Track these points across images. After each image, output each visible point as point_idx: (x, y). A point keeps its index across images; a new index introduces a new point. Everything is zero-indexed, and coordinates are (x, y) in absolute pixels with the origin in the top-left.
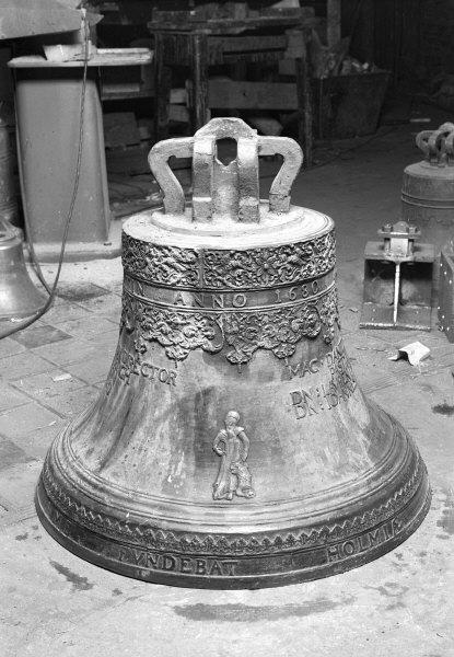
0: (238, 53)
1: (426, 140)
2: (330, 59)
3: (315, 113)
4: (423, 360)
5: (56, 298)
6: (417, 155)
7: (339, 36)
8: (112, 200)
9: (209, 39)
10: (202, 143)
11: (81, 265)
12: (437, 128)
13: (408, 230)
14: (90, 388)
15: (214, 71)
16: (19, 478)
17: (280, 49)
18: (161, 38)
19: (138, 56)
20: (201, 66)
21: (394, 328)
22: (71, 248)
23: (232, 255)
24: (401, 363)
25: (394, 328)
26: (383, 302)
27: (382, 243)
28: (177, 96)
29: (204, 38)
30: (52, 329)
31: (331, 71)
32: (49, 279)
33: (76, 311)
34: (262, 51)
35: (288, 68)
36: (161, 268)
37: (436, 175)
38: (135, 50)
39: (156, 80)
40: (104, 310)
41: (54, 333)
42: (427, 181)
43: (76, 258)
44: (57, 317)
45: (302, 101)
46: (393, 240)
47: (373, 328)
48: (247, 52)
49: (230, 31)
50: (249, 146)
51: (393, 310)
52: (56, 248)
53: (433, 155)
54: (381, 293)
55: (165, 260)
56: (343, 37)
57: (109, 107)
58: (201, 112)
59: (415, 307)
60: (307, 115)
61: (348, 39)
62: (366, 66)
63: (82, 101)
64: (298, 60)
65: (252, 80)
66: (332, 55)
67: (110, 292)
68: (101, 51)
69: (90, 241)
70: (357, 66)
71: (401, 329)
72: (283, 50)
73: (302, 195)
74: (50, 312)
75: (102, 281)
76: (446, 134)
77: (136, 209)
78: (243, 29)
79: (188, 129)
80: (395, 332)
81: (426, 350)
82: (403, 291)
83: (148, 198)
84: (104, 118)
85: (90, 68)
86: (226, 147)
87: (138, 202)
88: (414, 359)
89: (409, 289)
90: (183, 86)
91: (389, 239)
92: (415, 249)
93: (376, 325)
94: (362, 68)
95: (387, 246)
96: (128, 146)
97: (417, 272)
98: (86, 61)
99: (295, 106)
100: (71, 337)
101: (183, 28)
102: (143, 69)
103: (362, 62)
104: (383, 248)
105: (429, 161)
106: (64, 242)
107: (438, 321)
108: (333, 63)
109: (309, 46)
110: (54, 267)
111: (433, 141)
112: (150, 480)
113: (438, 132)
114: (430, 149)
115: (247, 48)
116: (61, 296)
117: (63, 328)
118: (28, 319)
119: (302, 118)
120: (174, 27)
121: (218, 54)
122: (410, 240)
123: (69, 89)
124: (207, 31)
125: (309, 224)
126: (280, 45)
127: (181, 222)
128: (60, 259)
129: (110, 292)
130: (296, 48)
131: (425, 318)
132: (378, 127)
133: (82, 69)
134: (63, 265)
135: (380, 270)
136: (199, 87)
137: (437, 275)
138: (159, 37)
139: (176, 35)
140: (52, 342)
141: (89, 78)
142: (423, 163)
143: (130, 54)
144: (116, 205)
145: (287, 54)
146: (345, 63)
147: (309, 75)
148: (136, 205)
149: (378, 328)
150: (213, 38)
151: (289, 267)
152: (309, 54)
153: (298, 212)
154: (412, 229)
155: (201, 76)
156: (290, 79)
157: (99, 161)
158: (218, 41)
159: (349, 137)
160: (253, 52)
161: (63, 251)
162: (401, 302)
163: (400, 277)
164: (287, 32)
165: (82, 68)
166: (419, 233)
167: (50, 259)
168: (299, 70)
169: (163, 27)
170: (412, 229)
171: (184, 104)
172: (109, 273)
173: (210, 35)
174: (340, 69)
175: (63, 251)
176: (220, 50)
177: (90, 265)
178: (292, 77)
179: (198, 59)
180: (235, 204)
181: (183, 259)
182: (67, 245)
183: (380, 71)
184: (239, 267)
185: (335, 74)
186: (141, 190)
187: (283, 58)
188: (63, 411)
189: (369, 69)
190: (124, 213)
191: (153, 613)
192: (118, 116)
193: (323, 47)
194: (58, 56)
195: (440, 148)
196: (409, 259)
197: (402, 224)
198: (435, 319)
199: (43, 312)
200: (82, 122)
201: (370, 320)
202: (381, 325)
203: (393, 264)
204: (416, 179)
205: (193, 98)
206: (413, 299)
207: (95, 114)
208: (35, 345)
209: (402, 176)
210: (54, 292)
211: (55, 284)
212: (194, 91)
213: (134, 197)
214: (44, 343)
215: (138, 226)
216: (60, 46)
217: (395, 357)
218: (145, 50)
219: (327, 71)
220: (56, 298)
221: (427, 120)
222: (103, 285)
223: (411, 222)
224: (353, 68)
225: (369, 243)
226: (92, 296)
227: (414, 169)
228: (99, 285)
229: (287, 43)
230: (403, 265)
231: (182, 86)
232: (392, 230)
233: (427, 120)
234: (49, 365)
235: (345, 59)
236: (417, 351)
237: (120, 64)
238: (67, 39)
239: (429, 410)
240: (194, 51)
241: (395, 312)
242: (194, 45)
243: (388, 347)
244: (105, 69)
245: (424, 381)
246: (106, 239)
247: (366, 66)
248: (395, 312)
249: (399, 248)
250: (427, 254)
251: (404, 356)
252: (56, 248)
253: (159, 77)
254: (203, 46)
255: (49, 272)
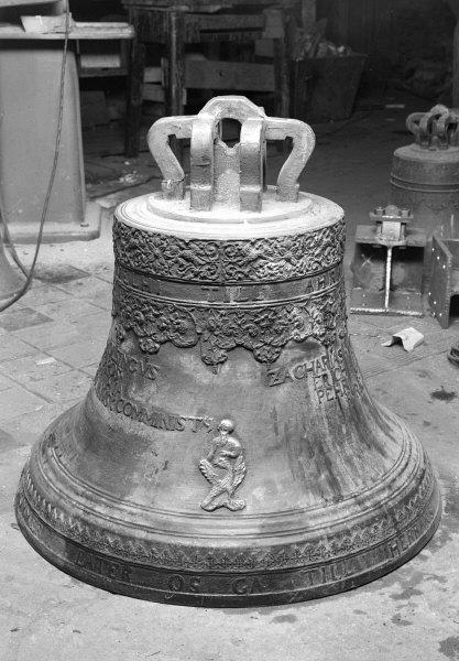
0: (215, 31)
1: (417, 122)
2: (306, 41)
3: (291, 97)
4: (418, 345)
5: (34, 280)
6: (407, 137)
7: (314, 19)
8: (87, 180)
9: (187, 17)
10: (201, 128)
11: (58, 247)
12: (427, 110)
13: (400, 214)
15: (190, 48)
16: (8, 464)
18: (135, 13)
19: (121, 31)
20: (177, 43)
22: (51, 228)
23: (253, 244)
24: (396, 349)
26: (375, 285)
27: (373, 227)
28: (152, 75)
29: (181, 16)
30: (31, 311)
31: (307, 54)
32: (27, 261)
33: (56, 293)
34: (240, 30)
35: (263, 48)
36: (177, 262)
37: (427, 158)
38: (115, 24)
39: (130, 57)
40: (84, 292)
41: (34, 316)
42: (417, 164)
43: (53, 240)
44: (36, 298)
46: (385, 224)
47: (364, 313)
50: (256, 126)
52: (33, 229)
54: (371, 278)
55: (181, 252)
56: (319, 17)
57: (88, 84)
58: (177, 92)
60: (285, 98)
61: (324, 21)
62: (341, 49)
64: (276, 40)
65: (227, 57)
66: (308, 37)
67: (89, 275)
68: (80, 25)
69: (67, 222)
70: (333, 48)
71: (393, 314)
72: (261, 29)
73: (314, 181)
74: (28, 295)
75: (80, 263)
76: (438, 117)
79: (193, 108)
81: (420, 336)
83: (122, 180)
84: (81, 95)
85: (70, 41)
86: (230, 130)
87: (111, 183)
88: (408, 345)
89: (402, 271)
91: (381, 223)
92: (407, 233)
93: (366, 310)
96: (97, 126)
98: (66, 33)
99: (272, 88)
100: (52, 320)
102: (123, 44)
103: (338, 46)
104: (375, 231)
106: (43, 222)
107: (428, 307)
109: (287, 27)
110: (31, 249)
111: (424, 125)
112: (171, 506)
113: (429, 115)
114: (421, 131)
116: (39, 278)
117: (43, 310)
118: (10, 299)
119: (280, 100)
121: (195, 32)
122: (402, 224)
125: (322, 213)
126: (258, 25)
127: (180, 206)
128: (39, 240)
129: (89, 275)
131: (416, 303)
132: (353, 112)
133: (62, 41)
134: (42, 246)
135: (374, 252)
136: (174, 65)
138: (134, 12)
139: (152, 11)
140: (34, 324)
142: (413, 146)
143: (99, 28)
145: (264, 34)
146: (321, 45)
147: (287, 56)
148: (109, 187)
152: (286, 34)
153: (308, 200)
154: (405, 212)
155: (177, 53)
156: (263, 60)
158: (195, 19)
159: (354, 111)
162: (393, 288)
163: (392, 262)
164: (265, 11)
165: (64, 41)
166: (412, 216)
167: (26, 241)
168: (277, 50)
170: (405, 212)
174: (316, 52)
176: (197, 28)
177: (67, 246)
179: (174, 36)
180: (238, 195)
181: (202, 252)
186: (114, 171)
187: (260, 38)
188: (49, 395)
189: (345, 51)
190: (97, 194)
192: (90, 89)
193: (298, 29)
194: (35, 27)
196: (401, 243)
197: (392, 208)
199: (22, 294)
200: (62, 97)
201: (360, 306)
202: (372, 310)
203: (384, 249)
204: (407, 163)
205: (168, 77)
206: (404, 285)
207: (74, 89)
208: (15, 328)
209: (390, 159)
210: (31, 274)
211: (33, 267)
213: (108, 178)
214: (24, 326)
215: (147, 213)
217: (389, 343)
218: (125, 24)
219: (303, 54)
220: (34, 280)
221: (402, 106)
222: (82, 268)
223: (401, 205)
224: (329, 51)
225: (359, 227)
226: (71, 278)
227: (403, 152)
228: (78, 267)
229: (265, 22)
230: (396, 249)
231: (158, 64)
232: (384, 213)
233: (402, 106)
235: (320, 42)
236: (411, 336)
239: (429, 398)
242: (170, 22)
244: (83, 42)
245: (419, 367)
246: (83, 220)
247: (341, 49)
248: (387, 297)
249: (391, 231)
250: (419, 239)
251: (398, 342)
252: (33, 229)
254: (180, 23)
255: (26, 254)
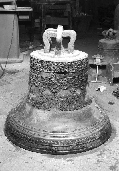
0: (53, 9)
1: (105, 33)
6: (103, 37)
11: (12, 64)
13: (100, 57)
14: (17, 97)
15: (46, 14)
17: (64, 9)
19: (29, 9)
20: (44, 13)
21: (96, 82)
22: (9, 60)
24: (99, 91)
25: (96, 82)
28: (37, 21)
29: (44, 5)
30: (5, 81)
31: (77, 15)
32: (4, 68)
33: (12, 76)
34: (60, 9)
38: (28, 8)
41: (6, 82)
42: (105, 44)
43: (11, 63)
45: (70, 24)
46: (96, 59)
48: (55, 9)
49: (51, 4)
51: (96, 77)
52: (5, 60)
53: (108, 37)
56: (80, 6)
58: (43, 25)
59: (102, 77)
62: (86, 14)
63: (12, 19)
64: (69, 12)
66: (77, 11)
69: (15, 58)
70: (84, 14)
71: (98, 82)
72: (65, 9)
73: (78, 46)
77: (26, 50)
78: (54, 3)
80: (97, 83)
82: (99, 73)
83: (29, 47)
88: (102, 90)
89: (101, 71)
90: (39, 18)
91: (95, 59)
92: (102, 62)
93: (91, 81)
94: (85, 15)
95: (95, 61)
97: (102, 67)
98: (15, 10)
99: (68, 24)
100: (11, 83)
101: (39, 2)
103: (85, 13)
104: (94, 61)
105: (106, 39)
108: (78, 13)
109: (72, 8)
110: (5, 65)
111: (107, 34)
115: (56, 8)
117: (8, 81)
120: (37, 2)
123: (12, 16)
124: (45, 3)
130: (69, 9)
136: (43, 18)
137: (107, 68)
139: (37, 4)
141: (16, 14)
142: (104, 39)
144: (21, 49)
146: (81, 13)
149: (92, 82)
150: (47, 5)
151: (61, 68)
152: (72, 10)
154: (102, 56)
155: (44, 15)
156: (66, 17)
157: (18, 36)
160: (57, 9)
161: (7, 59)
162: (98, 76)
163: (98, 69)
166: (103, 57)
169: (33, 2)
170: (102, 56)
171: (39, 23)
172: (26, 65)
173: (46, 5)
174: (79, 15)
175: (7, 59)
177: (15, 64)
178: (68, 17)
182: (8, 59)
183: (89, 15)
184: (46, 66)
185: (78, 16)
187: (65, 11)
189: (87, 15)
191: (37, 155)
193: (75, 9)
194: (7, 8)
195: (108, 35)
197: (98, 55)
198: (107, 80)
202: (93, 81)
203: (96, 65)
204: (102, 43)
212: (42, 19)
213: (26, 47)
214: (3, 85)
216: (8, 5)
217: (97, 90)
219: (76, 15)
221: (101, 29)
222: (18, 70)
223: (101, 54)
226: (16, 72)
227: (101, 41)
230: (99, 66)
233: (101, 29)
234: (5, 91)
235: (81, 12)
236: (103, 88)
237: (24, 11)
238: (9, 3)
239: (107, 104)
240: (42, 8)
241: (97, 78)
242: (42, 7)
243: (95, 87)
246: (19, 57)
247: (86, 14)
248: (97, 78)
250: (105, 63)
251: (99, 90)
252: (5, 60)
253: (32, 15)
